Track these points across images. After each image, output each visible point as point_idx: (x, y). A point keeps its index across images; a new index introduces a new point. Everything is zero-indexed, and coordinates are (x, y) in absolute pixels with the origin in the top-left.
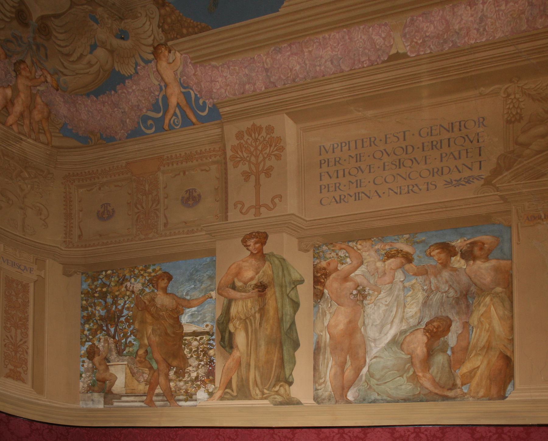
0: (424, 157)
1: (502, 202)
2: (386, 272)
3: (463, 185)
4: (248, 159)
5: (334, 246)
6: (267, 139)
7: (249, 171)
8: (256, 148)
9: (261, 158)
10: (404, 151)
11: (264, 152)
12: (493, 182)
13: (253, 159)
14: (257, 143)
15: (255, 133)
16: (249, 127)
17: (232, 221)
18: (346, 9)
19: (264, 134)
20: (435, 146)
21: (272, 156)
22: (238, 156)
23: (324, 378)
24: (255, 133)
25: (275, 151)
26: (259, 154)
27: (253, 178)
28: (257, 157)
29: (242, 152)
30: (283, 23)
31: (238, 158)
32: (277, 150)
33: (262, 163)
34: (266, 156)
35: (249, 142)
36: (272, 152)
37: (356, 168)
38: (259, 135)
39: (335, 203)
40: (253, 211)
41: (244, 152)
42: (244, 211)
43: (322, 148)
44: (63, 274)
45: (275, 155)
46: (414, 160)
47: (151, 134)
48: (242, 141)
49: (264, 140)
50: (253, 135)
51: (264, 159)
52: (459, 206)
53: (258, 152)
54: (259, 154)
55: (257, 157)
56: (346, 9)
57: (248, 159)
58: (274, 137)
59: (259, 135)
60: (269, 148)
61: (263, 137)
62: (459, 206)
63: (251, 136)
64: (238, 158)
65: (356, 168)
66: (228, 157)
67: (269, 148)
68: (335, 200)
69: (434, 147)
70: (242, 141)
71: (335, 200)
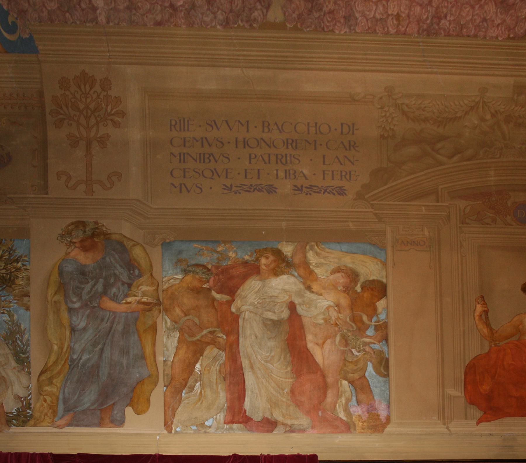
0: (225, 171)
1: (377, 220)
2: (238, 194)
3: (334, 194)
4: (76, 119)
5: (501, 14)
6: (101, 97)
9: (93, 121)
10: (319, 129)
11: (97, 114)
12: (366, 197)
13: (83, 121)
14: (89, 100)
15: (85, 85)
19: (97, 88)
20: (280, 160)
21: (108, 121)
22: (62, 112)
23: (70, 356)
24: (85, 85)
25: (113, 115)
28: (87, 118)
29: (67, 107)
31: (61, 114)
33: (95, 129)
35: (78, 96)
39: (263, 163)
40: (82, 187)
41: (70, 108)
43: (204, 139)
46: (214, 172)
47: (325, 190)
48: (67, 93)
49: (98, 96)
50: (83, 87)
51: (98, 123)
55: (87, 118)
57: (76, 119)
58: (78, 76)
59: (91, 88)
61: (97, 93)
63: (80, 87)
64: (61, 114)
66: (48, 110)
68: (344, 145)
69: (279, 161)
70: (67, 93)
71: (344, 145)
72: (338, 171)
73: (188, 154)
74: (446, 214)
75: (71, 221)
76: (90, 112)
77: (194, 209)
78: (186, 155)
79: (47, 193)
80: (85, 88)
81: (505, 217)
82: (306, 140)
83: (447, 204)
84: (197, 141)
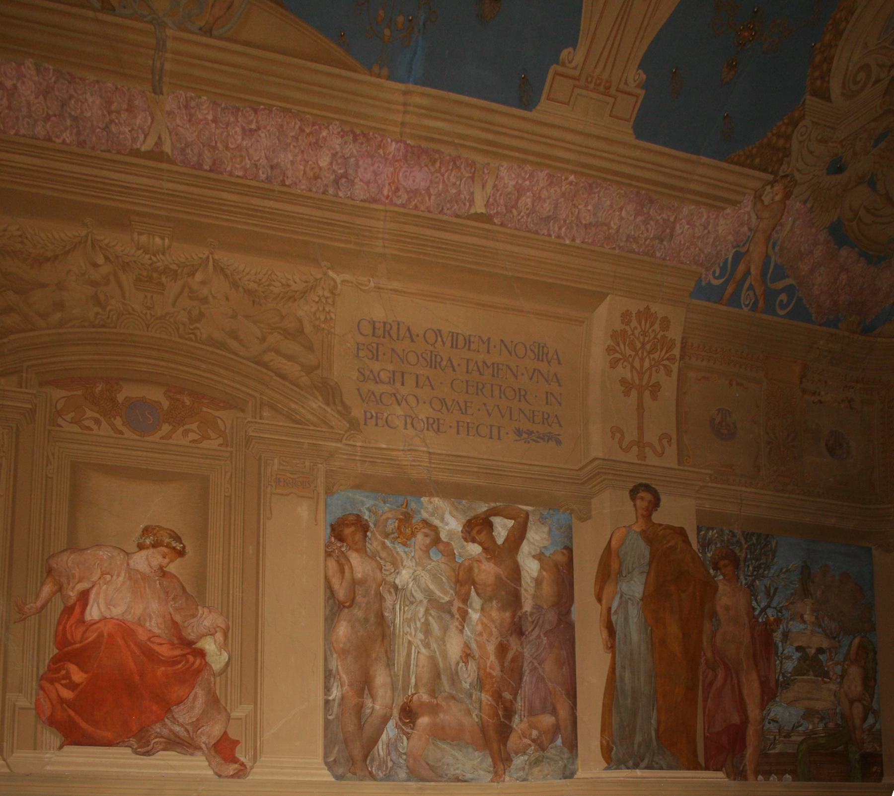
6: (659, 337)
7: (631, 382)
8: (643, 345)
11: (652, 356)
14: (647, 339)
16: (641, 310)
17: (650, 464)
18: (634, 162)
26: (646, 357)
27: (634, 393)
30: (505, 134)
31: (617, 352)
32: (668, 359)
33: (648, 374)
34: (653, 363)
35: (637, 332)
36: (663, 360)
37: (514, 390)
38: (651, 327)
42: (659, 450)
44: (332, 526)
45: (664, 366)
48: (627, 328)
50: (643, 323)
52: (665, 476)
53: (645, 354)
54: (646, 357)
55: (642, 360)
56: (634, 162)
57: (631, 360)
60: (659, 352)
62: (665, 476)
64: (617, 352)
65: (514, 390)
67: (659, 352)
70: (627, 328)
72: (539, 412)
73: (551, 393)
74: (30, 406)
75: (201, 444)
76: (645, 354)
77: (531, 465)
78: (549, 394)
79: (645, 461)
80: (645, 325)
81: (112, 419)
82: (507, 366)
83: (34, 392)
84: (488, 367)
